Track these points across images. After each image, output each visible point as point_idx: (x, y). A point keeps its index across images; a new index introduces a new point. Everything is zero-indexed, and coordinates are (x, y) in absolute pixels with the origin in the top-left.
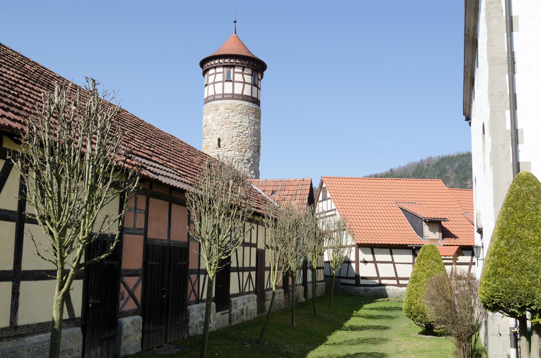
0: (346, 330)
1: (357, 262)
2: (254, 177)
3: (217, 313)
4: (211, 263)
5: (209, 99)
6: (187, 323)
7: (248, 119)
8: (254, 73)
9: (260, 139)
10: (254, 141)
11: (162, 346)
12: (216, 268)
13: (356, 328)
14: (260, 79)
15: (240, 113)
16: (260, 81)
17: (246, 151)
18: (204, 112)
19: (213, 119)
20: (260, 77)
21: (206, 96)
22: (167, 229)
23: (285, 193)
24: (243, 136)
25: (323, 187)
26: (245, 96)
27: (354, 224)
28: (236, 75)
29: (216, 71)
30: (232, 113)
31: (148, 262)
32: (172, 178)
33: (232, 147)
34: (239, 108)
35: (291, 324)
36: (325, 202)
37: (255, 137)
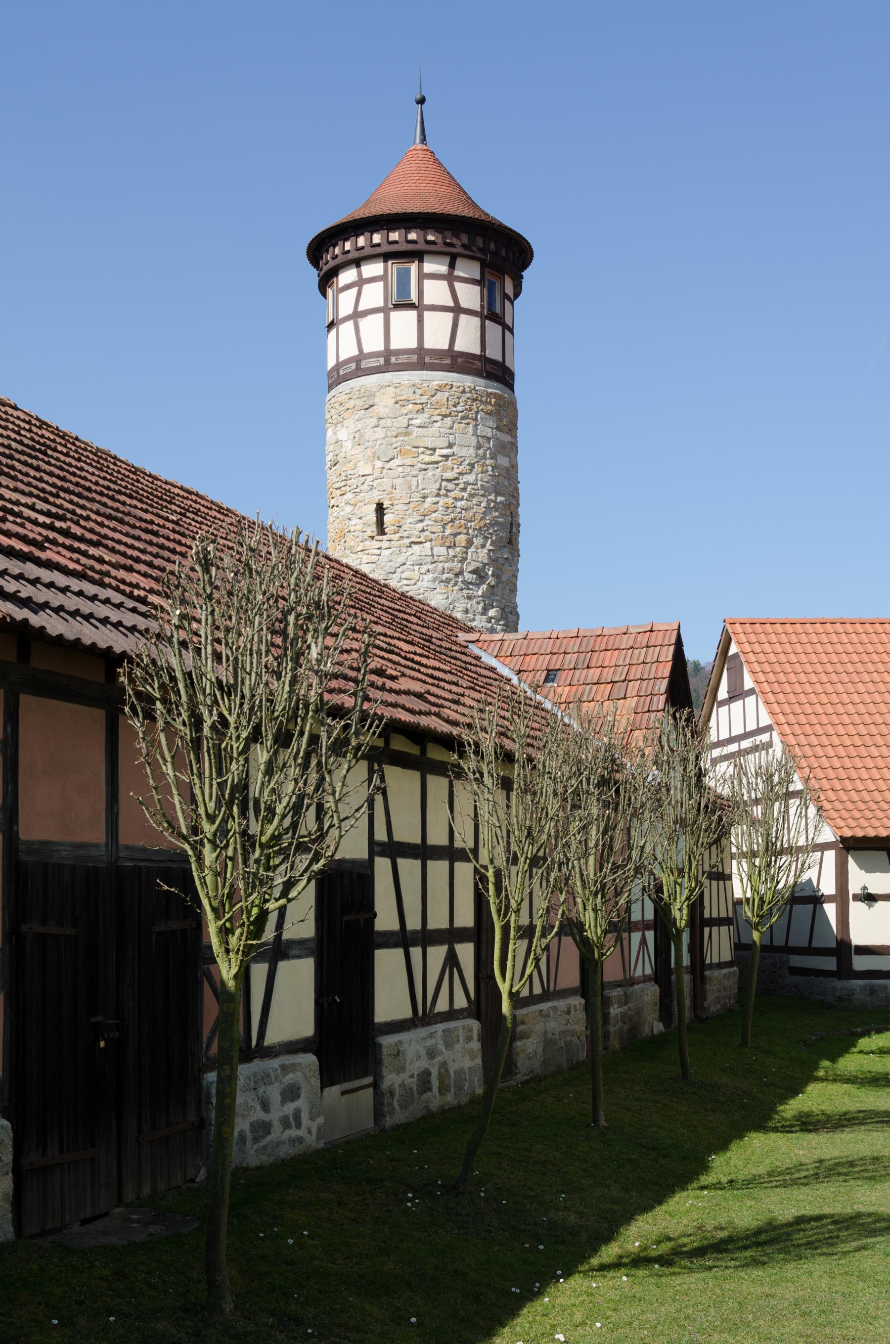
0: (787, 1129)
1: (842, 897)
2: (499, 627)
3: (327, 1090)
4: (228, 925)
5: (341, 373)
6: (204, 1131)
7: (475, 434)
8: (488, 277)
9: (517, 500)
10: (496, 509)
11: (106, 1215)
12: (242, 943)
13: (819, 1121)
14: (511, 295)
15: (445, 416)
16: (512, 304)
17: (470, 543)
18: (328, 416)
19: (358, 440)
20: (509, 289)
21: (331, 363)
22: (102, 806)
23: (590, 675)
24: (456, 493)
25: (731, 652)
26: (462, 354)
27: (820, 774)
28: (427, 283)
29: (360, 274)
30: (420, 416)
31: (24, 928)
32: (101, 621)
33: (423, 531)
34: (441, 397)
35: (591, 1120)
36: (737, 706)
37: (497, 494)
